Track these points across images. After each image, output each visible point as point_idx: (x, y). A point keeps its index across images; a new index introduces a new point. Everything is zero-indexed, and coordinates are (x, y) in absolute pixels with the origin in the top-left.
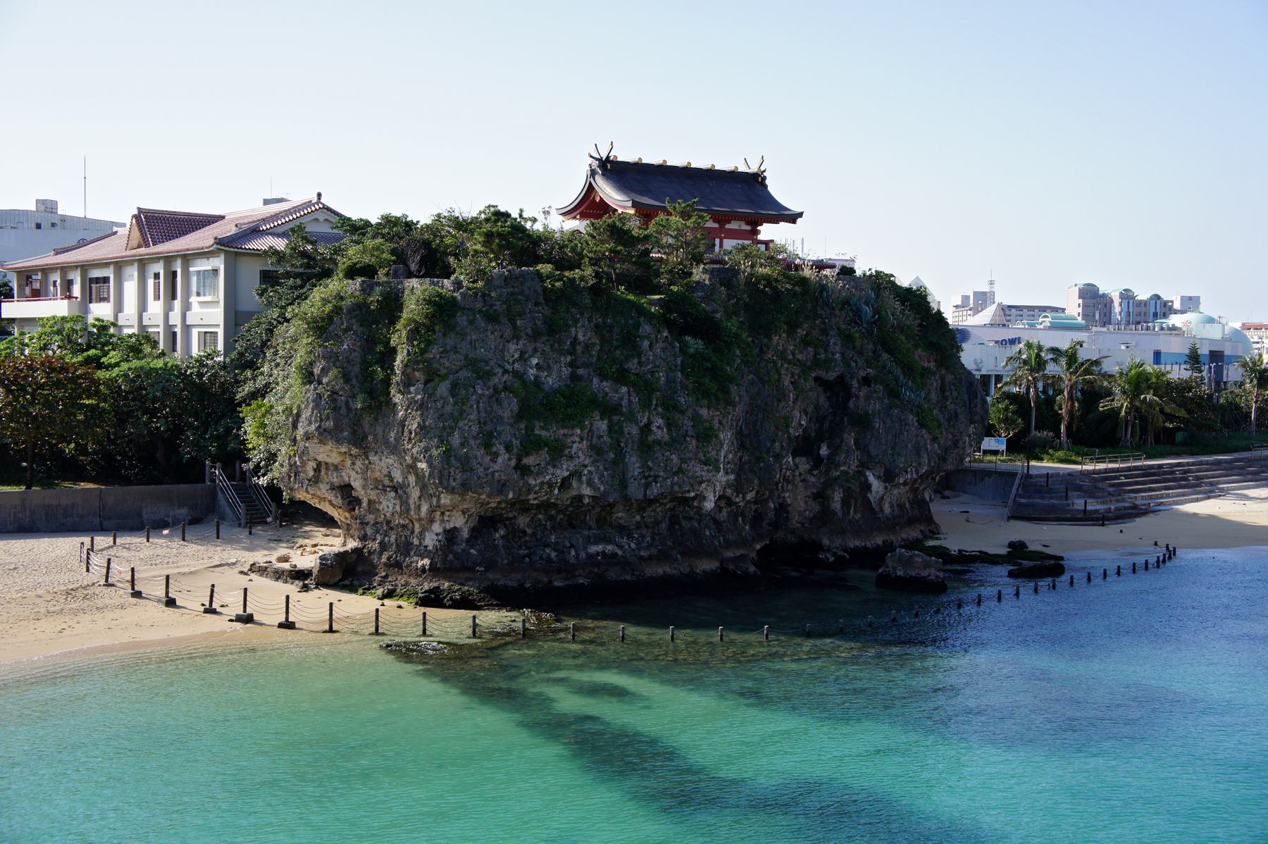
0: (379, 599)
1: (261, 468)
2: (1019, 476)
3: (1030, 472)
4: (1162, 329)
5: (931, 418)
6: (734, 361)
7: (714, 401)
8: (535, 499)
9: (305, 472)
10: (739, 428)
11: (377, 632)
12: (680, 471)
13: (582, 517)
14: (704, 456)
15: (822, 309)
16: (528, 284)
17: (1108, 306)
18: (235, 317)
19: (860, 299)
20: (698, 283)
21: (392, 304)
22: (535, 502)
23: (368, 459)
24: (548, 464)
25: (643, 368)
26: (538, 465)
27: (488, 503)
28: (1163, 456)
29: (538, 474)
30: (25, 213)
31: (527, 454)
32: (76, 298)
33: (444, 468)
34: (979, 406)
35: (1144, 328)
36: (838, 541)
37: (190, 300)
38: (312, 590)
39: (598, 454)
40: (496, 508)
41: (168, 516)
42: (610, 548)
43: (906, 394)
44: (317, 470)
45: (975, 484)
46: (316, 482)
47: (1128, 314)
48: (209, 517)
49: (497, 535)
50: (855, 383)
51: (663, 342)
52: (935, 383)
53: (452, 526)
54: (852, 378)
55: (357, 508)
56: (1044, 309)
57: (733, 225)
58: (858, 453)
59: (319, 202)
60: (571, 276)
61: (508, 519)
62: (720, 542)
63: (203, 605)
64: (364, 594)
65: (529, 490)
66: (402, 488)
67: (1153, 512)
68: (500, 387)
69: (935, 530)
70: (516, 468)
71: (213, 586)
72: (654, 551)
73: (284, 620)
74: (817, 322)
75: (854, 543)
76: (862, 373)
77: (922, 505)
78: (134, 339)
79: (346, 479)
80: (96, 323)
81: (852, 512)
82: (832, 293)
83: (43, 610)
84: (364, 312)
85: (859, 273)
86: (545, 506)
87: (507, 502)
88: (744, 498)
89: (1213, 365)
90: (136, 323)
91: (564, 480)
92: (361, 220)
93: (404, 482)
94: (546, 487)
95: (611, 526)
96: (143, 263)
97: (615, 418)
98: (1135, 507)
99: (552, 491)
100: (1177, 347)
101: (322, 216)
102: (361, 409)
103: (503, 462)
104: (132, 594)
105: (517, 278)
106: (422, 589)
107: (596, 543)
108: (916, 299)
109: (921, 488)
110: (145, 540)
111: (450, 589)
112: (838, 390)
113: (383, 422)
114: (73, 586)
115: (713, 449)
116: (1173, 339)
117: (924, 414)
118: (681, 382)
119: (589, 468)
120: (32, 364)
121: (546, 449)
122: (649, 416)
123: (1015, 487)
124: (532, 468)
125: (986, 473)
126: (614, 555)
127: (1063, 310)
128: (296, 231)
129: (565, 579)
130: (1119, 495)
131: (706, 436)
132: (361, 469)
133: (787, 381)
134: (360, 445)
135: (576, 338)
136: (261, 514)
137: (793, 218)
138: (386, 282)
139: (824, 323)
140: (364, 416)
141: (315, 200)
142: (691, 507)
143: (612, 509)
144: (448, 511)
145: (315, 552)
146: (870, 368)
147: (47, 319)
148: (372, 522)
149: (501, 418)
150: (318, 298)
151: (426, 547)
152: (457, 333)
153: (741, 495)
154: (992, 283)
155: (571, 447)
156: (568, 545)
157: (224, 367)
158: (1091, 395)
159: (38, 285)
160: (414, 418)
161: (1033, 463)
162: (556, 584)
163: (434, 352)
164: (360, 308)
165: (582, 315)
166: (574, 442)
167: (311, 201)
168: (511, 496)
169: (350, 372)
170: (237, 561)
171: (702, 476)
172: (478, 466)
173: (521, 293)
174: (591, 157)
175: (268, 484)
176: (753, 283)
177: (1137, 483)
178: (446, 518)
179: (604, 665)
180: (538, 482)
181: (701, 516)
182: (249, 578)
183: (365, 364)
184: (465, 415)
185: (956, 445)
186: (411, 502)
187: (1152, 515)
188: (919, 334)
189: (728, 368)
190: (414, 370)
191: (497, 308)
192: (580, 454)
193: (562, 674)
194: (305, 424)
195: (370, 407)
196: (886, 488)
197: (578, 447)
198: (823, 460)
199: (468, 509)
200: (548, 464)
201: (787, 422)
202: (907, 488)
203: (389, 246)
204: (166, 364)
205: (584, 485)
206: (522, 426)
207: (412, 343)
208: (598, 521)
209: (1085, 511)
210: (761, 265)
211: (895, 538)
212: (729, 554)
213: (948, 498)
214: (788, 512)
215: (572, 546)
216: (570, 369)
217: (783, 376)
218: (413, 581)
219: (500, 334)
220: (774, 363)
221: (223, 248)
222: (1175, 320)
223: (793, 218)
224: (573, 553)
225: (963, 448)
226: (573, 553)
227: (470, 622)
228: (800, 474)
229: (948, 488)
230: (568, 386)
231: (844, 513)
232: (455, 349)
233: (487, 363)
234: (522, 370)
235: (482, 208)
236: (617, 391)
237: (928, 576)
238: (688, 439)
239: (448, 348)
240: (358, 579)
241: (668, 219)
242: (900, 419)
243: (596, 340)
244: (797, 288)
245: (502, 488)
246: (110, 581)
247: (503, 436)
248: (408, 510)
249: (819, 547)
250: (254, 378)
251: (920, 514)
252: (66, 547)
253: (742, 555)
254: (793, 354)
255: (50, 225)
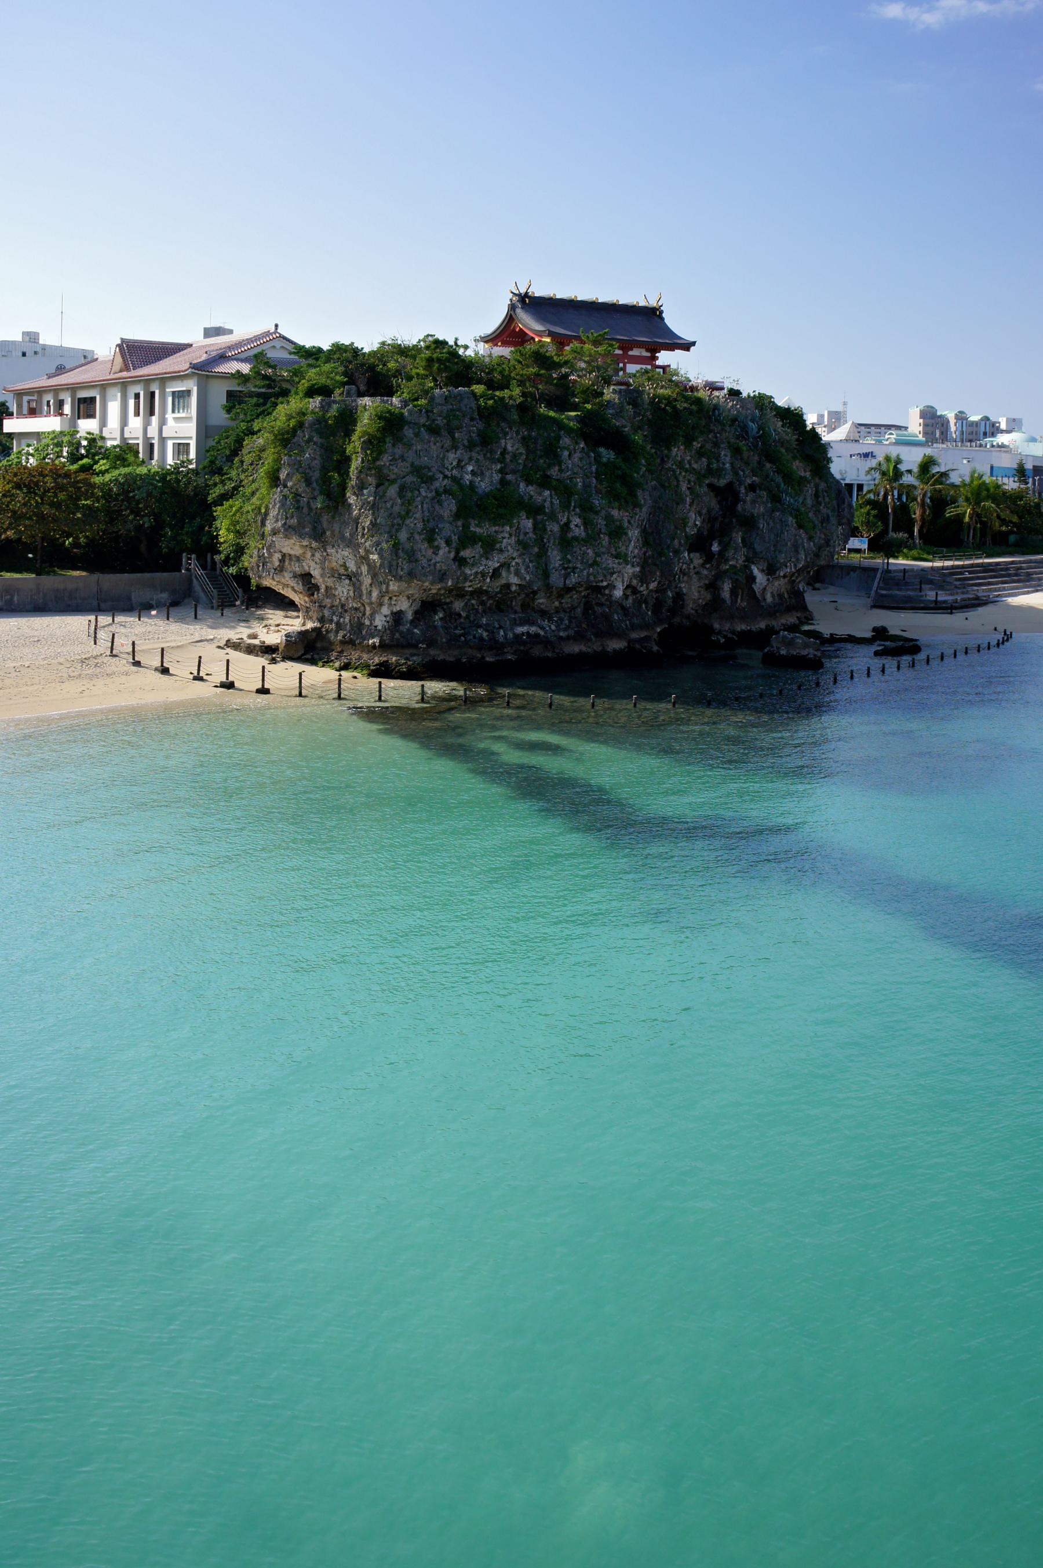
0: (336, 670)
1: (230, 559)
2: (880, 571)
3: (890, 568)
4: (993, 446)
5: (807, 520)
6: (641, 468)
7: (623, 503)
8: (469, 586)
9: (271, 562)
10: (643, 527)
11: (339, 697)
12: (595, 563)
13: (509, 603)
14: (616, 550)
15: (715, 425)
16: (465, 401)
17: (945, 425)
18: (204, 430)
19: (746, 417)
20: (609, 402)
21: (347, 420)
22: (470, 589)
23: (326, 551)
24: (481, 556)
25: (563, 475)
26: (473, 557)
27: (430, 589)
28: (999, 555)
29: (473, 565)
30: (14, 343)
31: (464, 548)
32: (67, 415)
33: (393, 559)
34: (846, 510)
35: (978, 445)
36: (727, 626)
37: (166, 416)
38: (279, 662)
39: (525, 548)
40: (437, 594)
41: (152, 599)
42: (533, 629)
43: (786, 500)
44: (282, 561)
45: (842, 577)
46: (281, 571)
47: (962, 433)
48: (186, 601)
49: (437, 617)
50: (743, 490)
51: (580, 452)
52: (810, 490)
53: (398, 609)
54: (740, 484)
55: (316, 593)
56: (889, 427)
57: (635, 352)
58: (744, 550)
59: (276, 331)
60: (502, 395)
61: (448, 604)
62: (626, 625)
63: (191, 673)
64: (323, 666)
65: (465, 578)
66: (355, 577)
67: (992, 602)
68: (441, 490)
69: (809, 617)
70: (455, 559)
71: (200, 657)
72: (571, 632)
73: (261, 687)
74: (710, 436)
75: (741, 627)
76: (749, 481)
77: (799, 595)
78: (118, 450)
79: (307, 568)
80: (88, 436)
81: (739, 600)
82: (723, 411)
83: (66, 675)
84: (322, 426)
85: (744, 395)
86: (478, 593)
87: (445, 589)
88: (647, 588)
89: (1037, 478)
90: (118, 435)
91: (495, 570)
92: (314, 347)
93: (357, 571)
94: (479, 576)
95: (533, 609)
96: (124, 385)
97: (539, 517)
98: (977, 598)
99: (484, 580)
100: (1007, 462)
101: (278, 344)
102: (321, 509)
103: (444, 554)
104: (133, 663)
105: (455, 397)
106: (373, 663)
107: (521, 624)
108: (793, 418)
109: (797, 581)
110: (137, 619)
111: (397, 663)
112: (727, 495)
113: (340, 520)
114: (86, 656)
115: (623, 545)
116: (1003, 455)
117: (802, 517)
118: (596, 487)
119: (517, 560)
120: (42, 471)
121: (480, 543)
122: (568, 516)
123: (877, 580)
124: (468, 560)
125: (851, 569)
126: (537, 635)
127: (906, 428)
128: (259, 358)
129: (496, 656)
130: (964, 588)
131: (617, 533)
132: (320, 559)
133: (684, 487)
134: (320, 539)
135: (505, 449)
136: (230, 598)
137: (687, 346)
138: (342, 401)
139: (716, 437)
140: (323, 514)
141: (273, 330)
142: (603, 595)
143: (535, 596)
144: (395, 596)
145: (278, 631)
146: (755, 476)
147: (48, 433)
148: (329, 605)
149: (442, 517)
150: (284, 412)
151: (376, 627)
152: (404, 444)
153: (645, 585)
154: (845, 404)
155: (502, 542)
156: (497, 626)
157: (195, 472)
158: (939, 502)
159: (34, 405)
160: (367, 516)
161: (891, 561)
162: (488, 659)
163: (385, 460)
164: (320, 422)
165: (511, 429)
166: (504, 538)
167: (269, 331)
168: (450, 583)
169: (311, 477)
170: (214, 638)
171: (613, 568)
172: (423, 558)
173: (459, 410)
174: (512, 292)
175: (237, 572)
176: (656, 403)
177: (978, 578)
178: (393, 603)
179: (539, 728)
180: (473, 572)
181: (611, 602)
182: (225, 651)
183: (324, 470)
184: (410, 515)
185: (827, 543)
186: (364, 588)
187: (991, 605)
188: (797, 447)
189: (635, 475)
190: (367, 475)
191: (439, 422)
192: (509, 548)
193: (505, 733)
194: (272, 522)
195: (328, 507)
196: (768, 580)
197: (507, 541)
198: (714, 555)
199: (412, 595)
200: (481, 556)
201: (684, 522)
202: (786, 580)
203: (341, 369)
204: (149, 471)
205: (512, 575)
206: (460, 523)
207: (366, 452)
208: (522, 606)
209: (936, 601)
210: (662, 387)
211: (776, 624)
212: (634, 635)
213: (819, 589)
214: (683, 600)
215: (501, 627)
216: (500, 475)
217: (681, 483)
218: (365, 656)
219: (441, 445)
220: (674, 471)
221: (196, 371)
222: (1002, 439)
223: (687, 346)
224: (502, 633)
225: (834, 547)
226: (502, 633)
227: (420, 689)
228: (694, 568)
229: (819, 581)
230: (499, 490)
231: (732, 601)
232: (403, 458)
233: (429, 469)
234: (459, 476)
235: (422, 338)
236: (540, 494)
237: (808, 655)
238: (602, 536)
239: (397, 456)
240: (318, 654)
241: (582, 347)
242: (781, 520)
243: (522, 450)
244: (693, 407)
245: (442, 577)
246: (114, 652)
247: (443, 532)
248: (361, 596)
249: (711, 630)
250: (222, 482)
251: (795, 602)
252: (77, 624)
253: (646, 636)
254: (690, 464)
255: (33, 353)
